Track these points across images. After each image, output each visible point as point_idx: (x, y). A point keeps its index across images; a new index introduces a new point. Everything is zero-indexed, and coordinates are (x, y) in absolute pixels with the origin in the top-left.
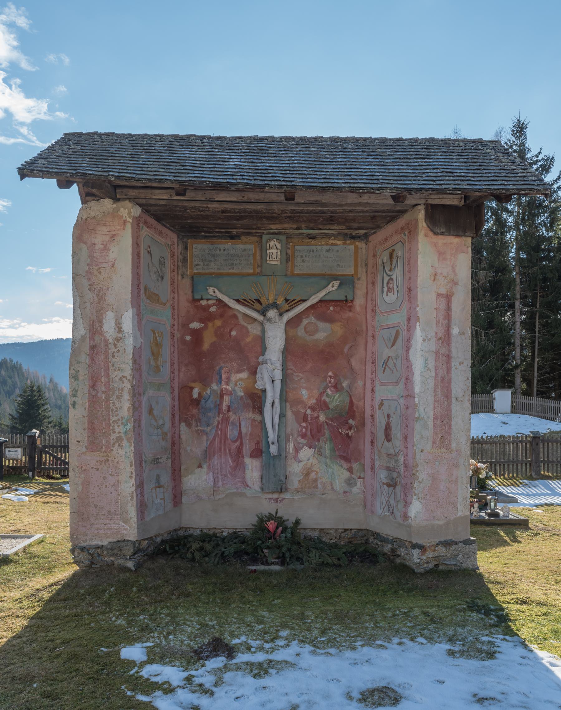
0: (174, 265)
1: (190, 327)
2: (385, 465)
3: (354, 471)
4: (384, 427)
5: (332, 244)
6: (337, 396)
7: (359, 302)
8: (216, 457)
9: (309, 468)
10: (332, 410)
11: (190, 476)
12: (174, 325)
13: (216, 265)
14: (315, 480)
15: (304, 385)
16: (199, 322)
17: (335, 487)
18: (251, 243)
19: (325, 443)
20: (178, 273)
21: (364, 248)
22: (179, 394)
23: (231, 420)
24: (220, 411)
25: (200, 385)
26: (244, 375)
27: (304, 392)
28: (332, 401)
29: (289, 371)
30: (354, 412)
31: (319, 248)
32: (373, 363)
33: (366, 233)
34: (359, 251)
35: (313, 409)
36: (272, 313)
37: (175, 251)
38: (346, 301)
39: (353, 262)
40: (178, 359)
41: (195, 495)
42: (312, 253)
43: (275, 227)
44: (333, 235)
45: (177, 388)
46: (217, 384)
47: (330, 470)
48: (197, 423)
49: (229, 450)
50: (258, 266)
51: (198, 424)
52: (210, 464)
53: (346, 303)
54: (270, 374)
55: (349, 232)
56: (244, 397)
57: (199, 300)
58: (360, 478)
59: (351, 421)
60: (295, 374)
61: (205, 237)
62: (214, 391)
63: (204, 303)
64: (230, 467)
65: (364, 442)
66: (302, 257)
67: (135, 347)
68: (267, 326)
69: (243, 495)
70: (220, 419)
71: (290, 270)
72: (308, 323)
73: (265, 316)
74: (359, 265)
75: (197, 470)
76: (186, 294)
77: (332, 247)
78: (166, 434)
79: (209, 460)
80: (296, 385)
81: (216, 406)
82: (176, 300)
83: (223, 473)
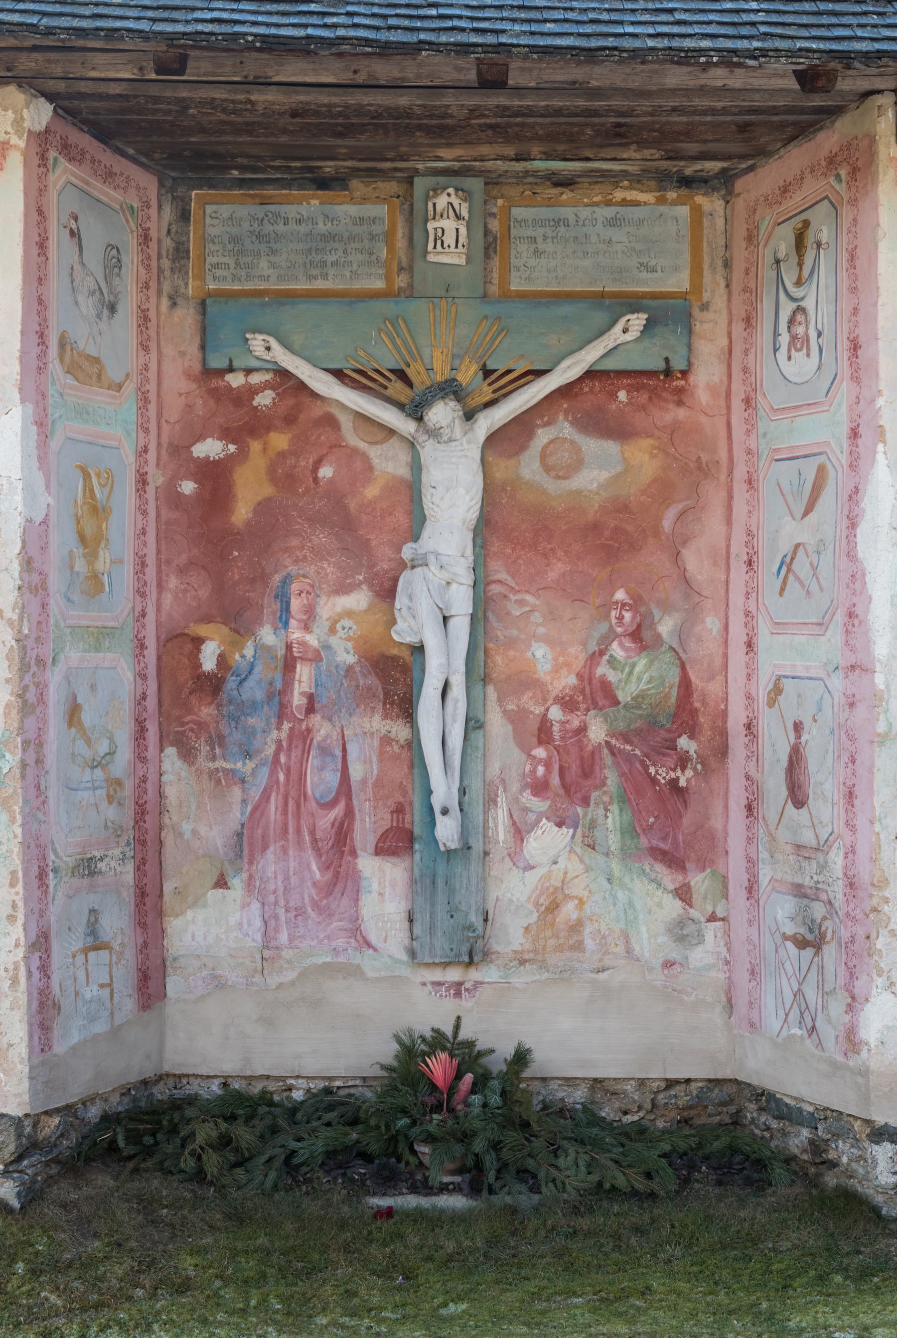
0: (148, 268)
1: (195, 455)
2: (789, 878)
3: (696, 898)
4: (785, 763)
5: (624, 203)
6: (642, 663)
7: (706, 376)
8: (270, 854)
9: (556, 889)
11: (190, 914)
12: (146, 450)
13: (273, 266)
14: (576, 927)
15: (541, 630)
16: (220, 439)
17: (637, 948)
18: (379, 200)
19: (606, 810)
20: (159, 292)
21: (722, 213)
22: (159, 658)
23: (318, 738)
24: (283, 712)
25: (225, 630)
26: (359, 600)
29: (495, 588)
30: (694, 713)
31: (585, 213)
32: (750, 563)
33: (724, 171)
34: (706, 222)
35: (568, 704)
36: (442, 413)
37: (153, 225)
38: (668, 372)
39: (687, 257)
40: (158, 552)
41: (205, 973)
42: (562, 229)
43: (449, 156)
44: (625, 174)
45: (154, 639)
48: (213, 749)
49: (312, 833)
50: (401, 269)
51: (218, 751)
52: (251, 877)
53: (665, 381)
54: (435, 603)
56: (357, 669)
57: (221, 373)
58: (712, 918)
59: (684, 742)
61: (241, 183)
62: (267, 649)
63: (236, 380)
64: (314, 884)
65: (726, 807)
66: (534, 240)
67: (29, 521)
68: (428, 450)
69: (356, 972)
70: (284, 735)
71: (496, 281)
72: (552, 442)
73: (420, 419)
74: (706, 266)
75: (215, 895)
76: (183, 354)
78: (119, 783)
79: (251, 862)
80: (515, 632)
82: (152, 374)
83: (292, 904)
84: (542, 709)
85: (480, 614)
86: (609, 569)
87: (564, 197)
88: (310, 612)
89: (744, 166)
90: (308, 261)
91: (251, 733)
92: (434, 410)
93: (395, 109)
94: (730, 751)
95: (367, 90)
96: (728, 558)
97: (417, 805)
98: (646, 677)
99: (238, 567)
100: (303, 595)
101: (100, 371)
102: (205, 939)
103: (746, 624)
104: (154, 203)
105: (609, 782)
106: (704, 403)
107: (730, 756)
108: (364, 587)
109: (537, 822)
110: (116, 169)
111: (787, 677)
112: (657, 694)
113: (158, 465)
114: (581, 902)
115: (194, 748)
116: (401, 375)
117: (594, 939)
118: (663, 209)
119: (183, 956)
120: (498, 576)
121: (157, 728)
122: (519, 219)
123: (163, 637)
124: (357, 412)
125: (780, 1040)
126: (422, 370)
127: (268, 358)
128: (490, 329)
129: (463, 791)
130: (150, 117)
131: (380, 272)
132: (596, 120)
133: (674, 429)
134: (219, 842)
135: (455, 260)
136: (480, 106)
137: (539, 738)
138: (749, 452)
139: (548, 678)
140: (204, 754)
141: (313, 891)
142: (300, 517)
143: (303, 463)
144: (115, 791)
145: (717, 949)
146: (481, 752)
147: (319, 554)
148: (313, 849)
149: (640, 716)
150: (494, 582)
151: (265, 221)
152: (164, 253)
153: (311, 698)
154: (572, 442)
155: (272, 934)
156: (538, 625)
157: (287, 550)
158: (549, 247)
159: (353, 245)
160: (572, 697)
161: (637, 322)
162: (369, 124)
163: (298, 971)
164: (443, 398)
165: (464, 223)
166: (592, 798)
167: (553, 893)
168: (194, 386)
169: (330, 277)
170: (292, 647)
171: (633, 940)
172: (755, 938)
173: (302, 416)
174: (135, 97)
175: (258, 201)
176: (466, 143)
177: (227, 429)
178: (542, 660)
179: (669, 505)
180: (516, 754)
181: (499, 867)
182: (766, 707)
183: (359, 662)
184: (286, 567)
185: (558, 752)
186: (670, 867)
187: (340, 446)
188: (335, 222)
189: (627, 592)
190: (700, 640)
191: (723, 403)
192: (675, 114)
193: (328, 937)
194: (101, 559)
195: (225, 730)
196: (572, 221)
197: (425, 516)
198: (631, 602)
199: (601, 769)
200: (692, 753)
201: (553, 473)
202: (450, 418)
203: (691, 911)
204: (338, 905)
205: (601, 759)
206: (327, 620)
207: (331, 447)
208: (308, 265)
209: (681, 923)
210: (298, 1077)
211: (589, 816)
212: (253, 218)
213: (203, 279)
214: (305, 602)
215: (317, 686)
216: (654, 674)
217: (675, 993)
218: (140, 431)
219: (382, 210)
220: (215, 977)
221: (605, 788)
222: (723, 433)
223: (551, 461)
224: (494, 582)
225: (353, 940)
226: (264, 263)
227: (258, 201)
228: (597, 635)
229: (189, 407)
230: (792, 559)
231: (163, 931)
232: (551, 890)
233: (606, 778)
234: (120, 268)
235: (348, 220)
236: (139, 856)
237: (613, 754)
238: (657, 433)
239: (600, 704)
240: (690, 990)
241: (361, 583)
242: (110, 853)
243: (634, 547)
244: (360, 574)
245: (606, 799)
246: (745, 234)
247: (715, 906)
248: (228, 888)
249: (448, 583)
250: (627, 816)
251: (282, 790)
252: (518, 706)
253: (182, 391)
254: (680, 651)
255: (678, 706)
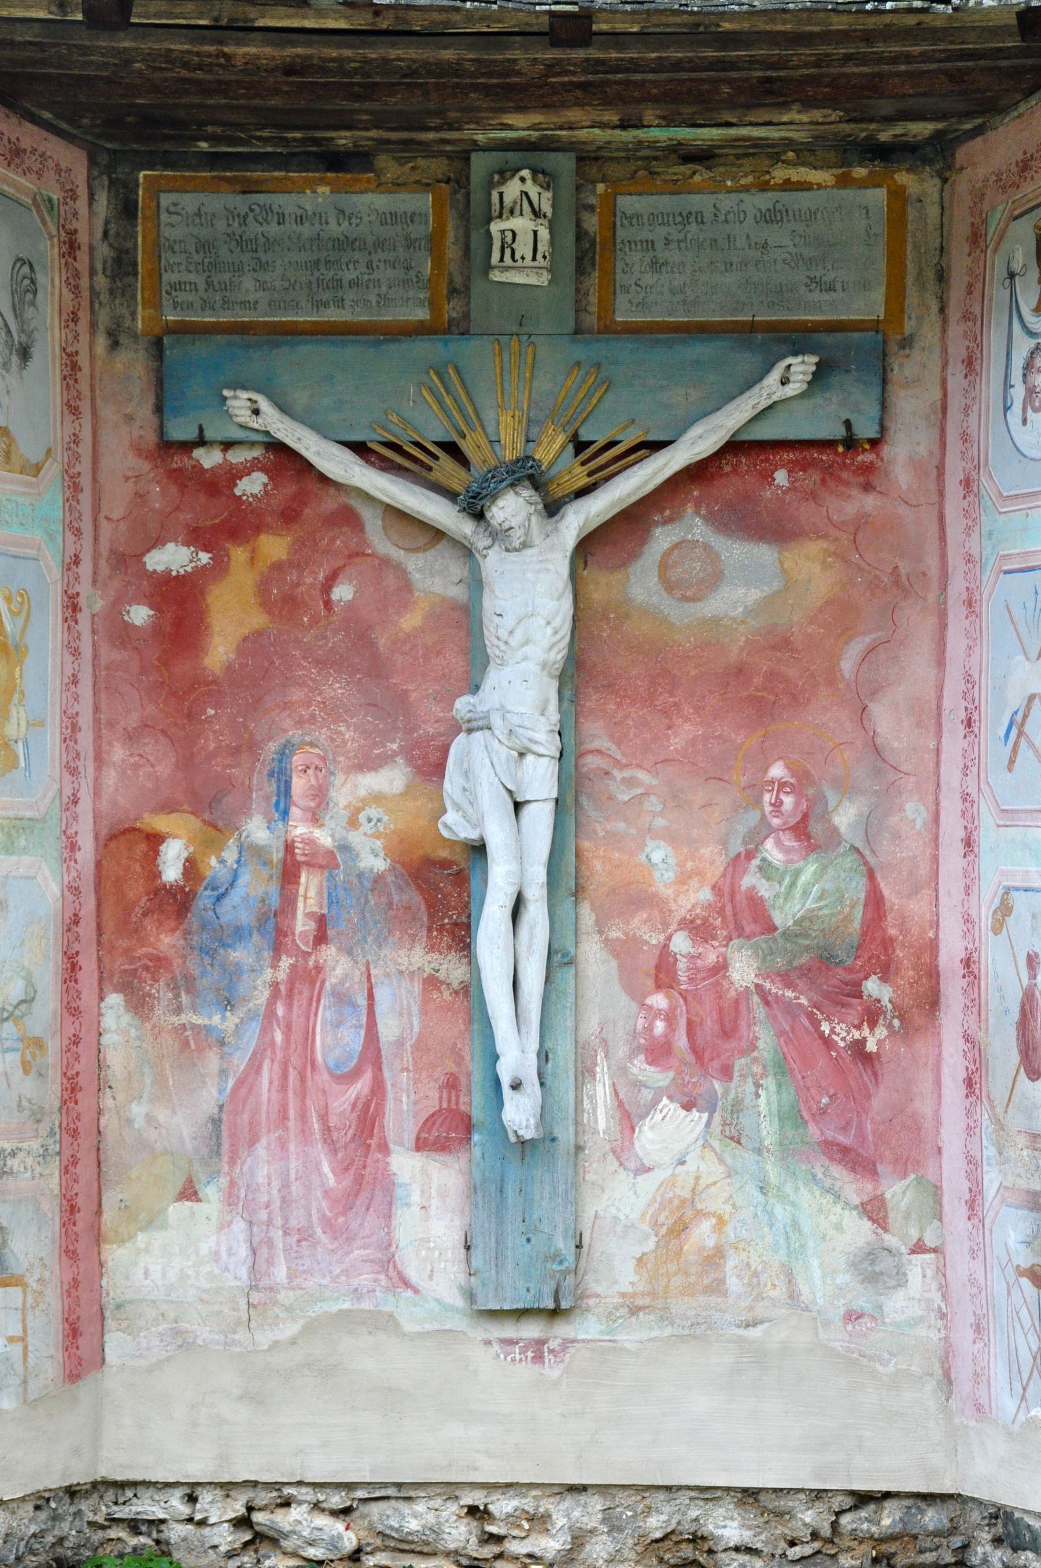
0: (76, 290)
1: (150, 567)
2: (1022, 1183)
3: (894, 1218)
4: (1015, 1015)
5: (788, 186)
6: (810, 870)
7: (905, 451)
8: (261, 1150)
9: (684, 1202)
10: (787, 935)
11: (141, 1238)
12: (76, 561)
13: (263, 286)
14: (715, 1257)
15: (660, 822)
16: (187, 544)
17: (804, 1290)
19: (758, 1085)
20: (93, 326)
21: (936, 197)
22: (98, 865)
24: (280, 942)
25: (195, 823)
26: (391, 779)
27: (657, 857)
28: (788, 895)
29: (592, 762)
30: (887, 944)
31: (727, 202)
32: (969, 723)
33: (938, 135)
34: (911, 213)
35: (699, 929)
36: (512, 508)
37: (81, 226)
38: (850, 443)
39: (882, 265)
40: (97, 709)
41: (163, 1326)
42: (693, 228)
43: (521, 125)
44: (789, 144)
45: (90, 836)
46: (270, 821)
47: (779, 1211)
48: (177, 996)
49: (324, 1118)
50: (453, 291)
51: (184, 998)
52: (232, 1184)
53: (849, 455)
54: (498, 783)
55: (860, 131)
56: (390, 879)
57: (187, 447)
58: (919, 1248)
59: (872, 987)
60: (618, 774)
61: (213, 160)
63: (209, 459)
64: (326, 1193)
65: (938, 1084)
66: (650, 245)
68: (494, 562)
69: (387, 1323)
70: (282, 975)
71: (594, 309)
72: (676, 546)
73: (479, 516)
74: (910, 280)
75: (178, 1211)
76: (129, 419)
77: (786, 197)
78: (39, 1044)
79: (232, 1162)
80: (621, 826)
81: (262, 920)
82: (85, 449)
83: (293, 1223)
84: (662, 937)
85: (570, 800)
86: (762, 732)
87: (697, 178)
88: (320, 795)
89: (968, 126)
90: (314, 280)
91: (233, 973)
92: (500, 503)
93: (436, 64)
94: (942, 1000)
95: (394, 38)
96: (939, 715)
97: (477, 1077)
98: (815, 890)
99: (215, 732)
100: (310, 772)
101: (9, 446)
102: (164, 1276)
103: (963, 813)
104: (83, 191)
105: (761, 1044)
106: (904, 487)
107: (943, 1007)
108: (400, 760)
109: (655, 1102)
110: (26, 144)
111: (1017, 889)
112: (833, 915)
113: (95, 581)
114: (721, 1222)
115: (149, 995)
116: (452, 449)
117: (740, 1277)
118: (847, 194)
119: (131, 1302)
120: (596, 744)
121: (94, 966)
122: (629, 213)
123: (104, 832)
124: (388, 506)
125: (1016, 1427)
126: (483, 442)
127: (256, 426)
128: (584, 381)
129: (544, 1056)
130: (76, 72)
131: (422, 296)
132: (734, 75)
133: (860, 523)
134: (186, 1133)
135: (533, 280)
136: (562, 60)
137: (657, 979)
138: (969, 559)
139: (670, 891)
140: (164, 1003)
141: (324, 1204)
142: (305, 658)
143: (309, 580)
144: (34, 1056)
145: (927, 1295)
146: (571, 999)
147: (334, 712)
148: (325, 1141)
149: (807, 948)
150: (591, 752)
151: (250, 219)
152: (99, 266)
153: (322, 922)
154: (706, 547)
155: (264, 1267)
156: (655, 815)
157: (286, 706)
158: (673, 256)
159: (381, 255)
160: (705, 920)
161: (801, 368)
162: (400, 84)
163: (302, 1322)
164: (512, 485)
165: (546, 222)
166: (736, 1068)
167: (678, 1208)
168: (146, 466)
169: (347, 303)
170: (294, 848)
171: (799, 1280)
172: (980, 1276)
173: (307, 511)
174: (55, 45)
175: (238, 188)
176: (544, 106)
177: (196, 530)
178: (661, 866)
179: (851, 638)
180: (624, 1003)
181: (597, 1167)
182: (990, 934)
183: (392, 869)
184: (285, 731)
185: (685, 999)
186: (853, 1170)
187: (363, 554)
188: (354, 221)
189: (787, 766)
190: (896, 836)
191: (933, 487)
192: (851, 63)
193: (346, 1272)
194: (14, 721)
195: (193, 966)
196: (708, 216)
197: (488, 657)
198: (793, 781)
199: (749, 1026)
200: (885, 1001)
201: (678, 593)
202: (524, 514)
203: (887, 1237)
204: (361, 1225)
205: (749, 1010)
206: (346, 807)
207: (350, 556)
208: (314, 286)
209: (871, 1255)
210: (300, 1483)
211: (732, 1095)
212: (231, 214)
213: (158, 306)
214: (313, 782)
215: (330, 904)
216: (829, 886)
217: (865, 1361)
218: (68, 534)
219: (425, 202)
220: (177, 1333)
221: (755, 1054)
222: (933, 531)
223: (675, 574)
224: (591, 752)
225: (382, 1277)
226: (248, 283)
227: (238, 188)
228: (742, 829)
229: (140, 497)
230: (1025, 717)
231: (101, 1265)
232: (676, 1203)
233: (757, 1039)
234: (35, 293)
235: (373, 218)
236: (68, 1153)
237: (767, 1003)
238: (834, 532)
239: (748, 929)
240: (886, 1356)
241: (395, 754)
242: (25, 1145)
243: (797, 700)
244: (393, 741)
245: (757, 1069)
246: (968, 231)
247: (922, 1230)
248: (199, 1200)
249: (522, 755)
250: (789, 1095)
251: (279, 1055)
252: (626, 934)
253: (130, 474)
254: (866, 852)
255: (864, 934)
